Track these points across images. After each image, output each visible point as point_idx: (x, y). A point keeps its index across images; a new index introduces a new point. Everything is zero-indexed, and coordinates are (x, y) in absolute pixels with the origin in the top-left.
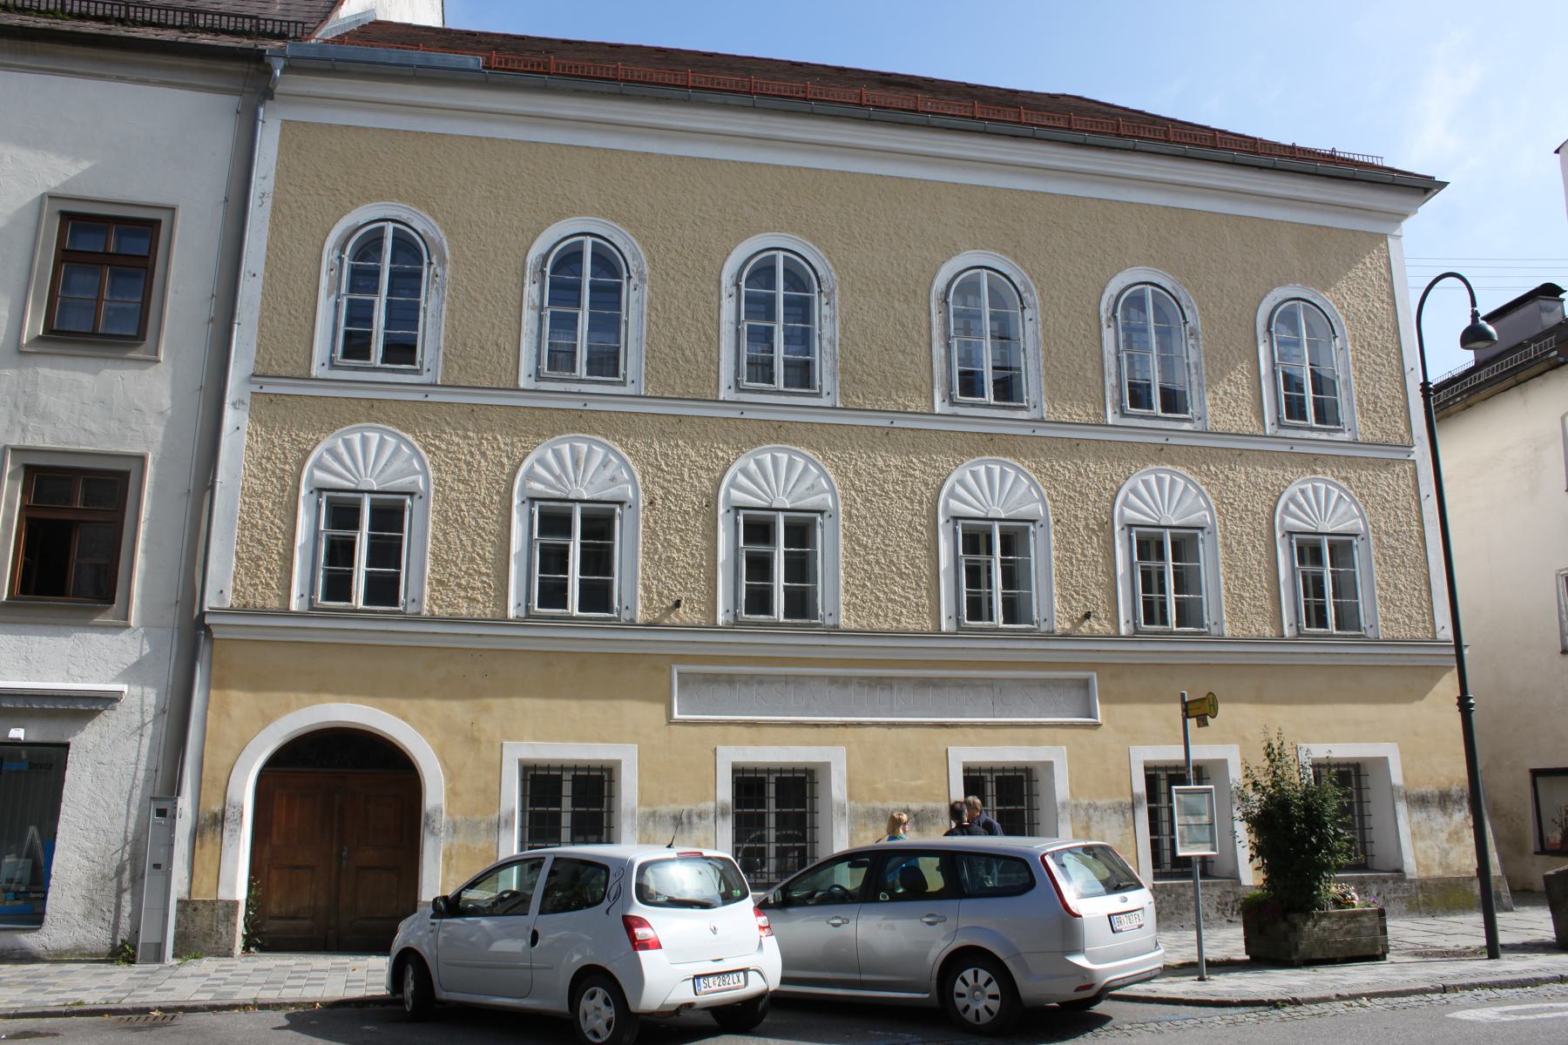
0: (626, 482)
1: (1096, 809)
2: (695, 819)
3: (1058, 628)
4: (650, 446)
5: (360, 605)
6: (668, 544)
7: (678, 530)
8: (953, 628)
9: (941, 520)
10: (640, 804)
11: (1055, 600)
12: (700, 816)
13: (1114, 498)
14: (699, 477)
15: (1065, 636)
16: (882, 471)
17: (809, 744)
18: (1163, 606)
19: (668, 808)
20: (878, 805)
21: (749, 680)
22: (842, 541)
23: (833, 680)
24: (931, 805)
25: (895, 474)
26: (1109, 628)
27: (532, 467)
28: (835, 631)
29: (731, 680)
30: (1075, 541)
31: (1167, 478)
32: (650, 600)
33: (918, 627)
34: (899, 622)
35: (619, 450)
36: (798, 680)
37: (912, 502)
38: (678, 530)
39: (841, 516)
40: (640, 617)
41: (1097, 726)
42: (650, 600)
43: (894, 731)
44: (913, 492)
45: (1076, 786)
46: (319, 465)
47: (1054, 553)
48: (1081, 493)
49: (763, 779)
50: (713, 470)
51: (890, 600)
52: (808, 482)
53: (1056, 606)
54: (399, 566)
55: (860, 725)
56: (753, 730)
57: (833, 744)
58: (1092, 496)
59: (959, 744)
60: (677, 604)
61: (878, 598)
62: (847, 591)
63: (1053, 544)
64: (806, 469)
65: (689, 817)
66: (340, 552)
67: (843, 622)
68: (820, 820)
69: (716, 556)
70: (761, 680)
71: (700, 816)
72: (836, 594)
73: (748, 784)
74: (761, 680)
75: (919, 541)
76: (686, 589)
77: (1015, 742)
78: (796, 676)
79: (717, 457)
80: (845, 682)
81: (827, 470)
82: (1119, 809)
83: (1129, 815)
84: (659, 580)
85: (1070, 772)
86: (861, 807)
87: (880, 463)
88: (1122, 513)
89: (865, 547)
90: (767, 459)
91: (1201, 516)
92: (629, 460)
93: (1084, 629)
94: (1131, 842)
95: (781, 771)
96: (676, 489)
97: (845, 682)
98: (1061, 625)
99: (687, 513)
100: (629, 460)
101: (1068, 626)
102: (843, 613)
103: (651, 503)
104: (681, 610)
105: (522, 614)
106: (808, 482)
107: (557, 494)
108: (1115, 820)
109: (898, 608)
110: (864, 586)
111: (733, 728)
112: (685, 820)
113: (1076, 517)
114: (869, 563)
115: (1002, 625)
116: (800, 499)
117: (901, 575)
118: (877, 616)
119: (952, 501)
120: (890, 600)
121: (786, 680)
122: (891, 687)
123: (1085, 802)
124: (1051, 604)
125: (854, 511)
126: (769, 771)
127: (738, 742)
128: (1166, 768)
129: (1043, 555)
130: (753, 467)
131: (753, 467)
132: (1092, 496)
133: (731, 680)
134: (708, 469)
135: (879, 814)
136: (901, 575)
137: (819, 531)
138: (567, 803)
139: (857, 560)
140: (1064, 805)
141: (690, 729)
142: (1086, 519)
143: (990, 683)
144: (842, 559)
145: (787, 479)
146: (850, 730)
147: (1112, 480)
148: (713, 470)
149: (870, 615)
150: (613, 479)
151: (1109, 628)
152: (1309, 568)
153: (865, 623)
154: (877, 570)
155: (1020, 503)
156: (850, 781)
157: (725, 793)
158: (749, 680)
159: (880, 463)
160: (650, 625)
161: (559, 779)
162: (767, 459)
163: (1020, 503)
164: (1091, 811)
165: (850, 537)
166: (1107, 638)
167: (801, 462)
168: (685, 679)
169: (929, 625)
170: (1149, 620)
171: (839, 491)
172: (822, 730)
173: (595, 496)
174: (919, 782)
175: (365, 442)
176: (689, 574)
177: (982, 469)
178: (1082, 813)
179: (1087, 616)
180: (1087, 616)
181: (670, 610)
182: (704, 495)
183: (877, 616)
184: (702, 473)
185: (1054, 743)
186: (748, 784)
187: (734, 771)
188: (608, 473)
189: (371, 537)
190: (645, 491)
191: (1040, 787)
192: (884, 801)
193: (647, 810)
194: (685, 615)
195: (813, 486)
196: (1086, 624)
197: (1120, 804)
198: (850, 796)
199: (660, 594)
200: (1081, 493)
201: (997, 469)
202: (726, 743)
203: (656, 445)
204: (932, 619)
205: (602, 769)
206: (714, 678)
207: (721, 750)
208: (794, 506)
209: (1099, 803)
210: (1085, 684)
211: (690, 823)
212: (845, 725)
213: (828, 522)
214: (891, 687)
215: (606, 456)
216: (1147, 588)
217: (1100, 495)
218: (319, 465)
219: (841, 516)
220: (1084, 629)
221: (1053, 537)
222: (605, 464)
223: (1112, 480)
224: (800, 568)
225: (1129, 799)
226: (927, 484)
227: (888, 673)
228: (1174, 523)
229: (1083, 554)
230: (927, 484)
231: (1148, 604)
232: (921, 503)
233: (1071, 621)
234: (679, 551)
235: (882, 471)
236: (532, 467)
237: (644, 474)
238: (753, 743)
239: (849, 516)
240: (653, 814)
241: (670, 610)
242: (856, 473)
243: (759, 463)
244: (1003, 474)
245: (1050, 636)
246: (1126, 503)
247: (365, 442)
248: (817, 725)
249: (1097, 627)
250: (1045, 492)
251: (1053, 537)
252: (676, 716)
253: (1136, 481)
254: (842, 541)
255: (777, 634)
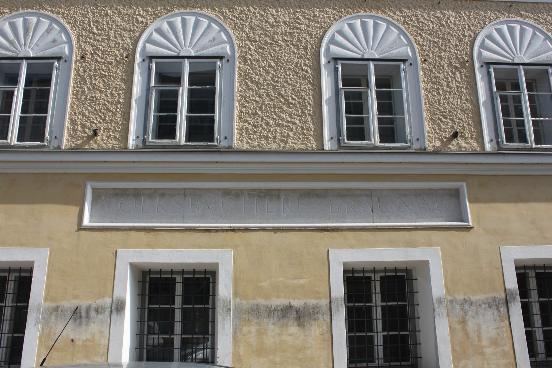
0: (65, 43)
1: (471, 304)
2: (93, 314)
3: (429, 146)
4: (85, 16)
5: (183, 142)
6: (94, 87)
7: (101, 77)
8: (335, 147)
9: (323, 61)
10: (46, 299)
11: (426, 123)
12: (97, 311)
13: (473, 43)
14: (121, 36)
15: (436, 152)
16: (272, 26)
17: (200, 247)
18: (521, 124)
19: (69, 304)
20: (261, 301)
21: (152, 194)
22: (237, 79)
23: (226, 193)
24: (313, 302)
25: (284, 28)
26: (475, 145)
27: (333, 36)
28: (230, 150)
29: (137, 194)
30: (441, 76)
31: (518, 27)
32: (75, 130)
33: (304, 147)
34: (286, 142)
35: (61, 20)
36: (196, 193)
37: (298, 48)
38: (101, 77)
39: (237, 60)
40: (65, 144)
41: (468, 228)
42: (75, 130)
43: (279, 234)
44: (299, 41)
45: (451, 284)
46: (149, 40)
47: (422, 86)
48: (443, 39)
49: (369, 278)
50: (133, 31)
51: (278, 125)
52: (211, 36)
53: (427, 128)
54: (213, 112)
55: (247, 230)
56: (151, 235)
57: (222, 247)
58: (454, 41)
59: (340, 246)
60: (95, 133)
61: (267, 124)
62: (240, 119)
63: (421, 78)
64: (209, 26)
65: (88, 310)
66: (356, 106)
67: (236, 144)
68: (421, 311)
69: (131, 94)
70: (163, 194)
71: (97, 311)
72: (231, 122)
73: (357, 282)
74: (163, 194)
75: (304, 78)
76: (104, 121)
77: (392, 244)
78: (194, 189)
79: (137, 21)
80: (237, 194)
81: (227, 27)
82: (493, 304)
83: (503, 309)
84: (84, 115)
85: (445, 271)
86: (245, 304)
87: (271, 20)
88: (480, 54)
89: (257, 84)
90: (178, 21)
91: (404, 51)
92: (68, 27)
93: (453, 146)
94: (506, 335)
95: (385, 270)
96: (102, 46)
97: (237, 194)
98: (432, 143)
99: (111, 63)
100: (68, 27)
101: (438, 144)
102: (236, 136)
103: (83, 57)
104: (99, 138)
105: (141, 145)
106: (211, 36)
107: (10, 54)
108: (490, 315)
109: (285, 132)
110: (256, 114)
111: (133, 234)
112: (83, 314)
113: (440, 57)
114: (260, 96)
115: (378, 144)
116: (203, 49)
117: (289, 104)
118: (267, 138)
119: (148, 45)
120: (278, 125)
121: (185, 193)
122: (279, 197)
123: (460, 297)
124: (422, 125)
125: (249, 57)
126: (374, 271)
127: (138, 246)
128: (534, 268)
129: (413, 90)
130: (165, 27)
131: (165, 27)
132: (454, 41)
133: (137, 194)
134: (130, 31)
135: (262, 309)
136: (289, 104)
137: (402, 74)
138: (178, 301)
139: (250, 94)
140: (440, 301)
141: (96, 234)
142: (449, 58)
143: (369, 194)
144: (236, 93)
145: (193, 35)
146: (237, 234)
147: (470, 29)
148: (133, 31)
149: (260, 137)
150: (54, 41)
151: (475, 145)
152: (509, 93)
153: (256, 144)
154: (267, 101)
155: (392, 47)
156: (236, 280)
157: (338, 289)
158: (152, 194)
159: (271, 20)
160: (72, 151)
161: (173, 281)
162: (178, 21)
163: (392, 47)
164: (467, 306)
165: (244, 76)
166: (474, 153)
167: (205, 22)
168: (97, 195)
169: (313, 145)
170: (510, 139)
171: (236, 42)
172: (212, 234)
173: (40, 54)
174: (302, 281)
175: (184, 23)
176: (109, 110)
177: (358, 23)
178: (458, 308)
179: (455, 135)
180: (455, 135)
181: (90, 138)
182: (125, 49)
183: (267, 138)
184: (126, 34)
185: (430, 244)
186: (357, 282)
187: (345, 272)
188: (50, 37)
189: (191, 92)
190: (78, 49)
191: (418, 285)
192: (267, 298)
193: (52, 305)
194: (102, 141)
195: (214, 39)
196: (454, 142)
197: (494, 299)
198: (236, 294)
199: (83, 126)
200: (443, 39)
201: (370, 22)
202: (126, 246)
203: (91, 16)
204: (316, 140)
205: (205, 272)
206: (125, 191)
207: (120, 252)
208: (198, 54)
209: (474, 298)
210: (456, 194)
211: (88, 316)
212: (233, 230)
213: (226, 65)
214: (279, 197)
215: (50, 25)
216: (506, 113)
217: (460, 41)
218: (149, 40)
219: (237, 60)
220: (453, 146)
221: (421, 73)
222: (49, 31)
223: (470, 29)
224: (388, 104)
225: (503, 295)
226: (310, 35)
227: (277, 186)
228: (526, 62)
229: (448, 86)
230: (310, 35)
231: (160, 120)
232: (305, 48)
233: (440, 140)
234: (101, 92)
235: (272, 26)
236: (333, 36)
237: (79, 36)
238: (150, 246)
239: (244, 60)
240: (56, 309)
241: (90, 138)
242: (251, 28)
243: (171, 24)
244: (376, 26)
245: (423, 152)
246: (482, 46)
247: (184, 23)
248: (208, 230)
249: (464, 145)
250: (412, 38)
251: (421, 73)
252: (86, 222)
253: (490, 29)
254: (237, 79)
255: (182, 155)
